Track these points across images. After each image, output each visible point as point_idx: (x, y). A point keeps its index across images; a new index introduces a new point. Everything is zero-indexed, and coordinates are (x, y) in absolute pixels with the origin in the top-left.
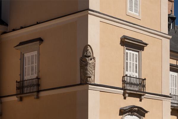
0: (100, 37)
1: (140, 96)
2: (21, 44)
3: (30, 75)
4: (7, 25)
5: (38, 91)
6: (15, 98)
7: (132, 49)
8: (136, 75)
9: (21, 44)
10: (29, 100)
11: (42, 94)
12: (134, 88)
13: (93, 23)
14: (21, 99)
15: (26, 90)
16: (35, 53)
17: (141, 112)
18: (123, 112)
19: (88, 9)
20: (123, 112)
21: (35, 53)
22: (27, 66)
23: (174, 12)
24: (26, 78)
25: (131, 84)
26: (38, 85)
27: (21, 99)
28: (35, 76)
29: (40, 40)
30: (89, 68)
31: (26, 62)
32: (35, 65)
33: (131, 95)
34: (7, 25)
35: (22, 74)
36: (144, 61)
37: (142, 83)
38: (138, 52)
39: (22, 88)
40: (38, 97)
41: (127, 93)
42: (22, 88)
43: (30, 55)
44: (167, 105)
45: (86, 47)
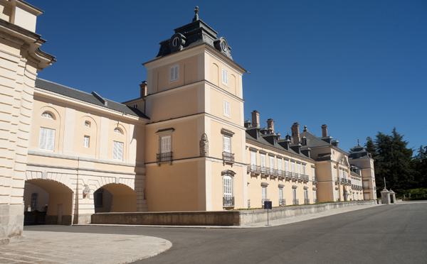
0: (211, 129)
1: (231, 164)
2: (160, 131)
3: (166, 150)
4: (149, 119)
5: (172, 160)
6: (156, 164)
7: (120, 114)
8: (229, 151)
9: (160, 131)
10: (165, 166)
11: (174, 162)
12: (228, 159)
13: (207, 120)
14: (160, 165)
15: (163, 159)
16: (170, 137)
17: (232, 174)
18: (223, 174)
19: (204, 113)
20: (223, 174)
21: (170, 137)
22: (163, 145)
23: (71, 200)
24: (163, 152)
25: (227, 157)
26: (172, 157)
27: (160, 165)
28: (169, 151)
29: (173, 129)
30: (205, 147)
31: (163, 142)
32: (169, 144)
33: (227, 163)
34: (149, 119)
35: (160, 149)
36: (233, 142)
37: (232, 157)
38: (304, 164)
39: (160, 159)
40: (171, 164)
41: (225, 163)
42: (160, 159)
43: (166, 138)
44: (245, 168)
45: (203, 135)
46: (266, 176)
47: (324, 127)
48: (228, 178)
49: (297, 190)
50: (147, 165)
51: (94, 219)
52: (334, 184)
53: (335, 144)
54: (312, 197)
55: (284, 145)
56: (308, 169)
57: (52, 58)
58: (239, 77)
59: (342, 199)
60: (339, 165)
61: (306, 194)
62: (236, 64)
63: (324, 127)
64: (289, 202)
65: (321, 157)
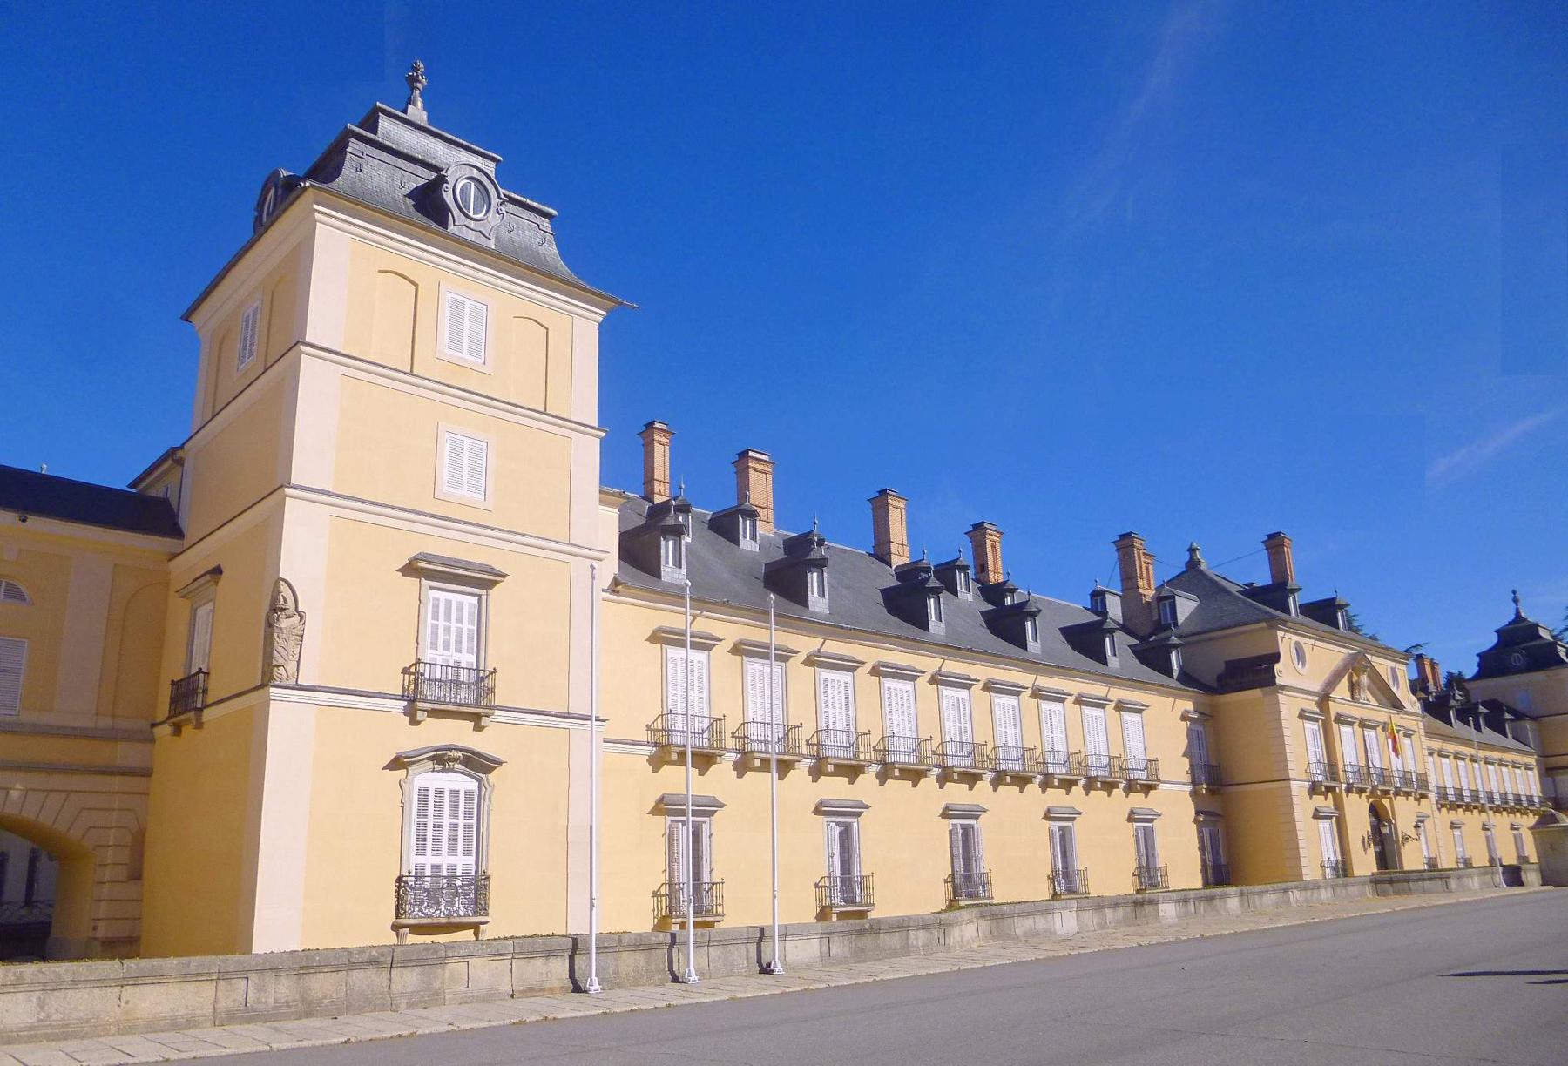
1: (476, 719)
20: (398, 763)
46: (704, 760)
47: (1274, 543)
48: (461, 782)
49: (1077, 827)
50: (156, 730)
51: (1375, 881)
52: (1299, 788)
53: (1324, 613)
54: (1182, 859)
55: (1086, 641)
56: (1154, 727)
57: (879, 502)
58: (578, 329)
59: (1365, 863)
60: (1334, 709)
61: (1518, 841)
62: (587, 263)
63: (1274, 543)
64: (1480, 859)
65: (1228, 678)
